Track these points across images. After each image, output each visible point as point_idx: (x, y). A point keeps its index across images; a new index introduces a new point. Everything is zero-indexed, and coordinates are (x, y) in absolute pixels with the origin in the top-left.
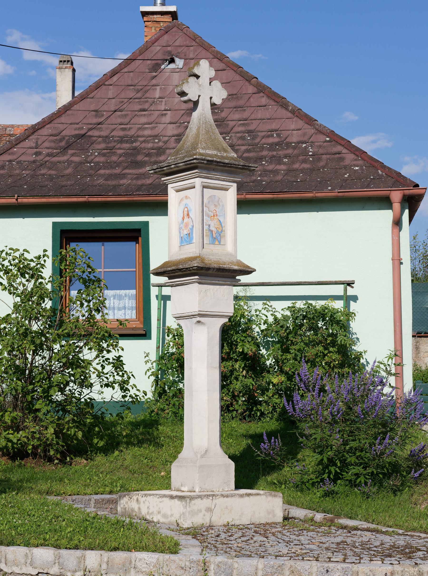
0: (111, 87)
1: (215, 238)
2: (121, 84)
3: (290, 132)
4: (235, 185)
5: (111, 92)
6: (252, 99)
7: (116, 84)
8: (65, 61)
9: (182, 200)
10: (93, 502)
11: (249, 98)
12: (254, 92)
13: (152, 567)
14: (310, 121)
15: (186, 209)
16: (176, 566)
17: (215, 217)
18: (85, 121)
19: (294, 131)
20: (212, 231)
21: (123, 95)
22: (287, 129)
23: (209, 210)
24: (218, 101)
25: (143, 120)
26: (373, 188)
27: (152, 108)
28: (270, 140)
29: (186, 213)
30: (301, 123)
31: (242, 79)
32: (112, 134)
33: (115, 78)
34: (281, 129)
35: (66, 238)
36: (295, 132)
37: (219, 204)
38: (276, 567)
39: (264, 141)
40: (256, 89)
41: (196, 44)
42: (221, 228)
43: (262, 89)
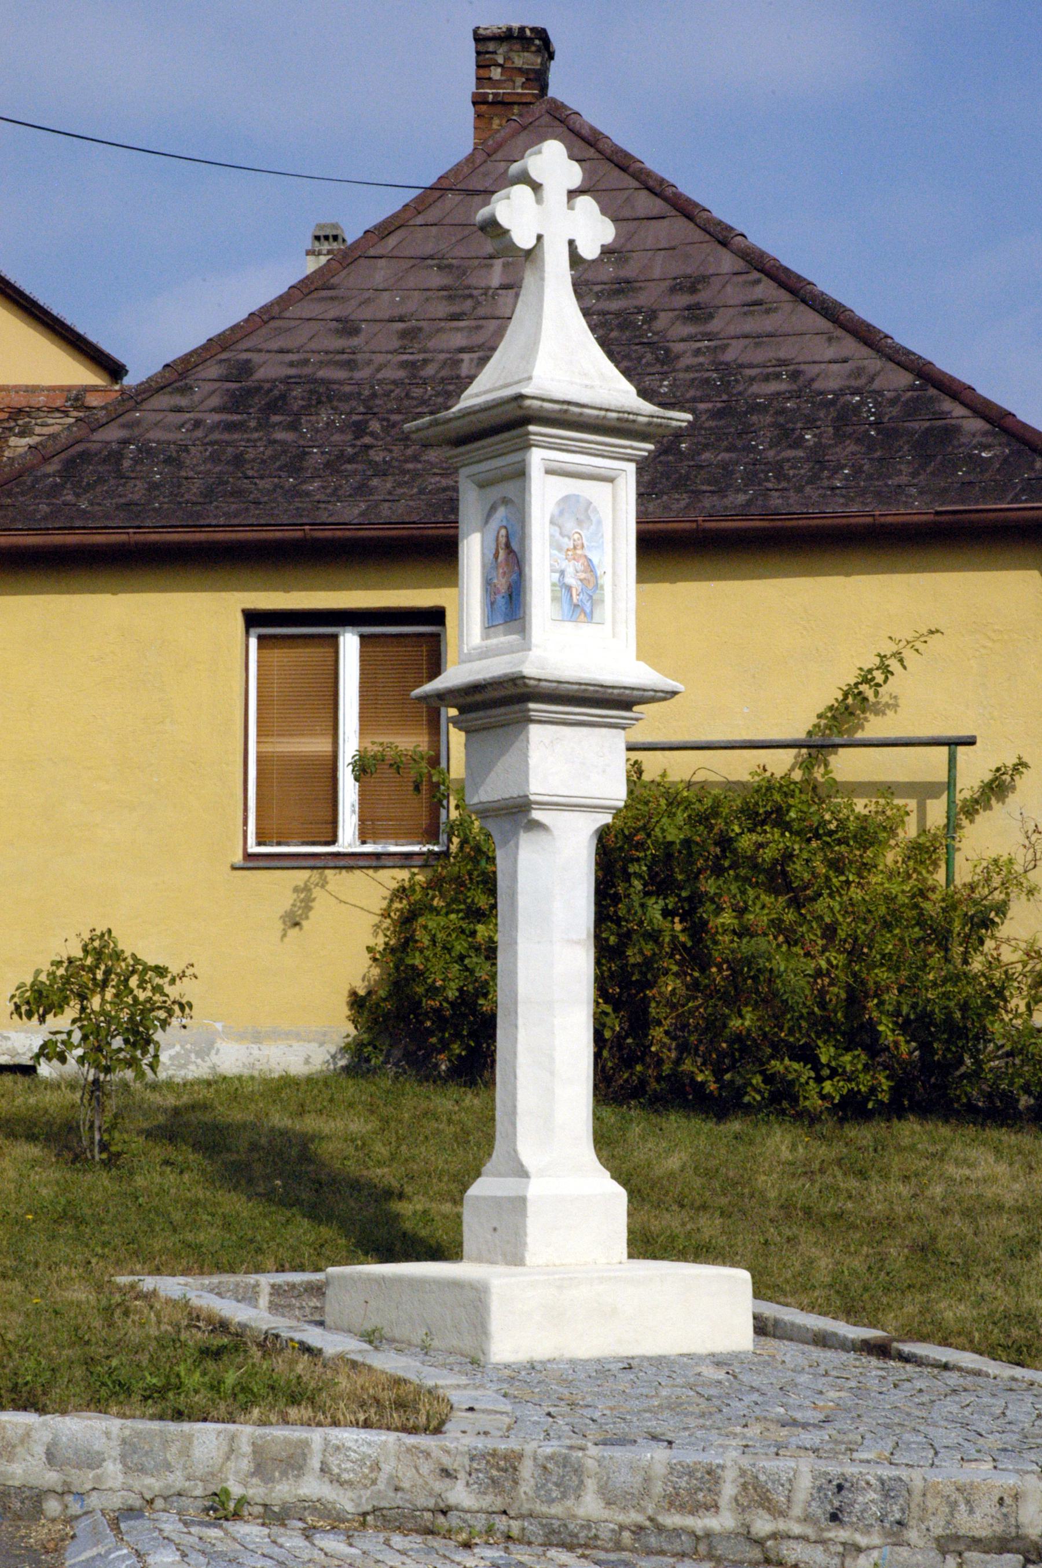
0: (382, 262)
1: (576, 606)
2: (407, 253)
3: (823, 366)
4: (632, 467)
5: (381, 273)
6: (729, 289)
7: (395, 253)
8: (326, 238)
9: (493, 509)
10: (265, 1291)
11: (724, 286)
12: (735, 270)
13: (366, 1471)
14: (865, 335)
15: (503, 532)
16: (432, 1467)
17: (579, 552)
18: (313, 345)
19: (831, 364)
20: (569, 588)
21: (411, 282)
22: (817, 358)
23: (561, 534)
24: (590, 251)
25: (459, 340)
26: (1026, 501)
27: (481, 311)
28: (773, 387)
29: (503, 540)
30: (850, 346)
31: (708, 237)
32: (379, 376)
33: (392, 241)
34: (800, 359)
35: (260, 638)
36: (835, 367)
37: (589, 518)
38: (699, 1475)
39: (755, 388)
40: (742, 263)
41: (597, 155)
42: (592, 579)
43: (760, 265)
